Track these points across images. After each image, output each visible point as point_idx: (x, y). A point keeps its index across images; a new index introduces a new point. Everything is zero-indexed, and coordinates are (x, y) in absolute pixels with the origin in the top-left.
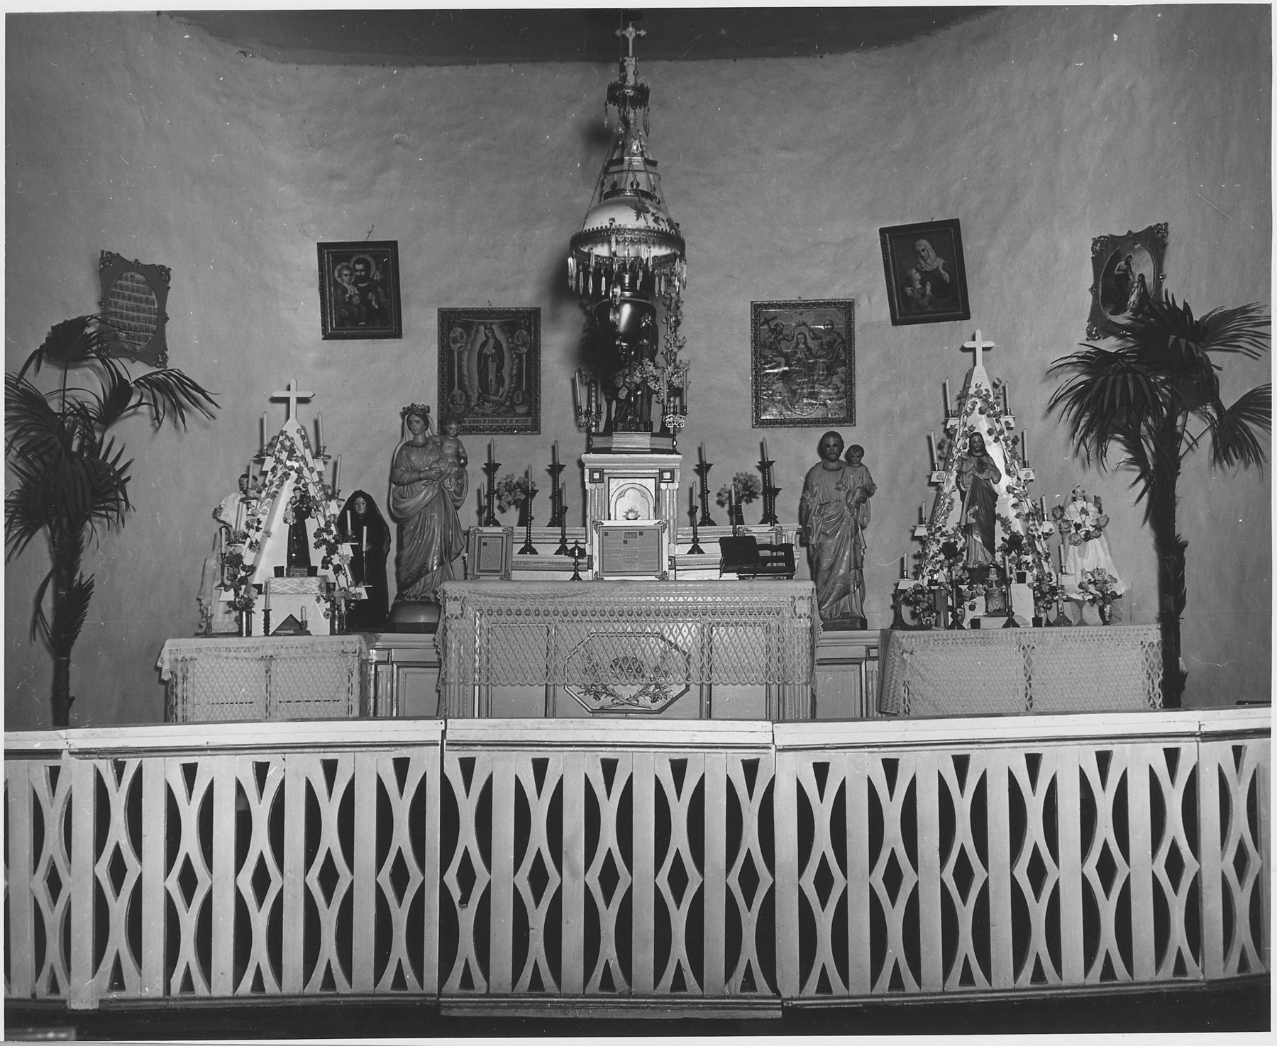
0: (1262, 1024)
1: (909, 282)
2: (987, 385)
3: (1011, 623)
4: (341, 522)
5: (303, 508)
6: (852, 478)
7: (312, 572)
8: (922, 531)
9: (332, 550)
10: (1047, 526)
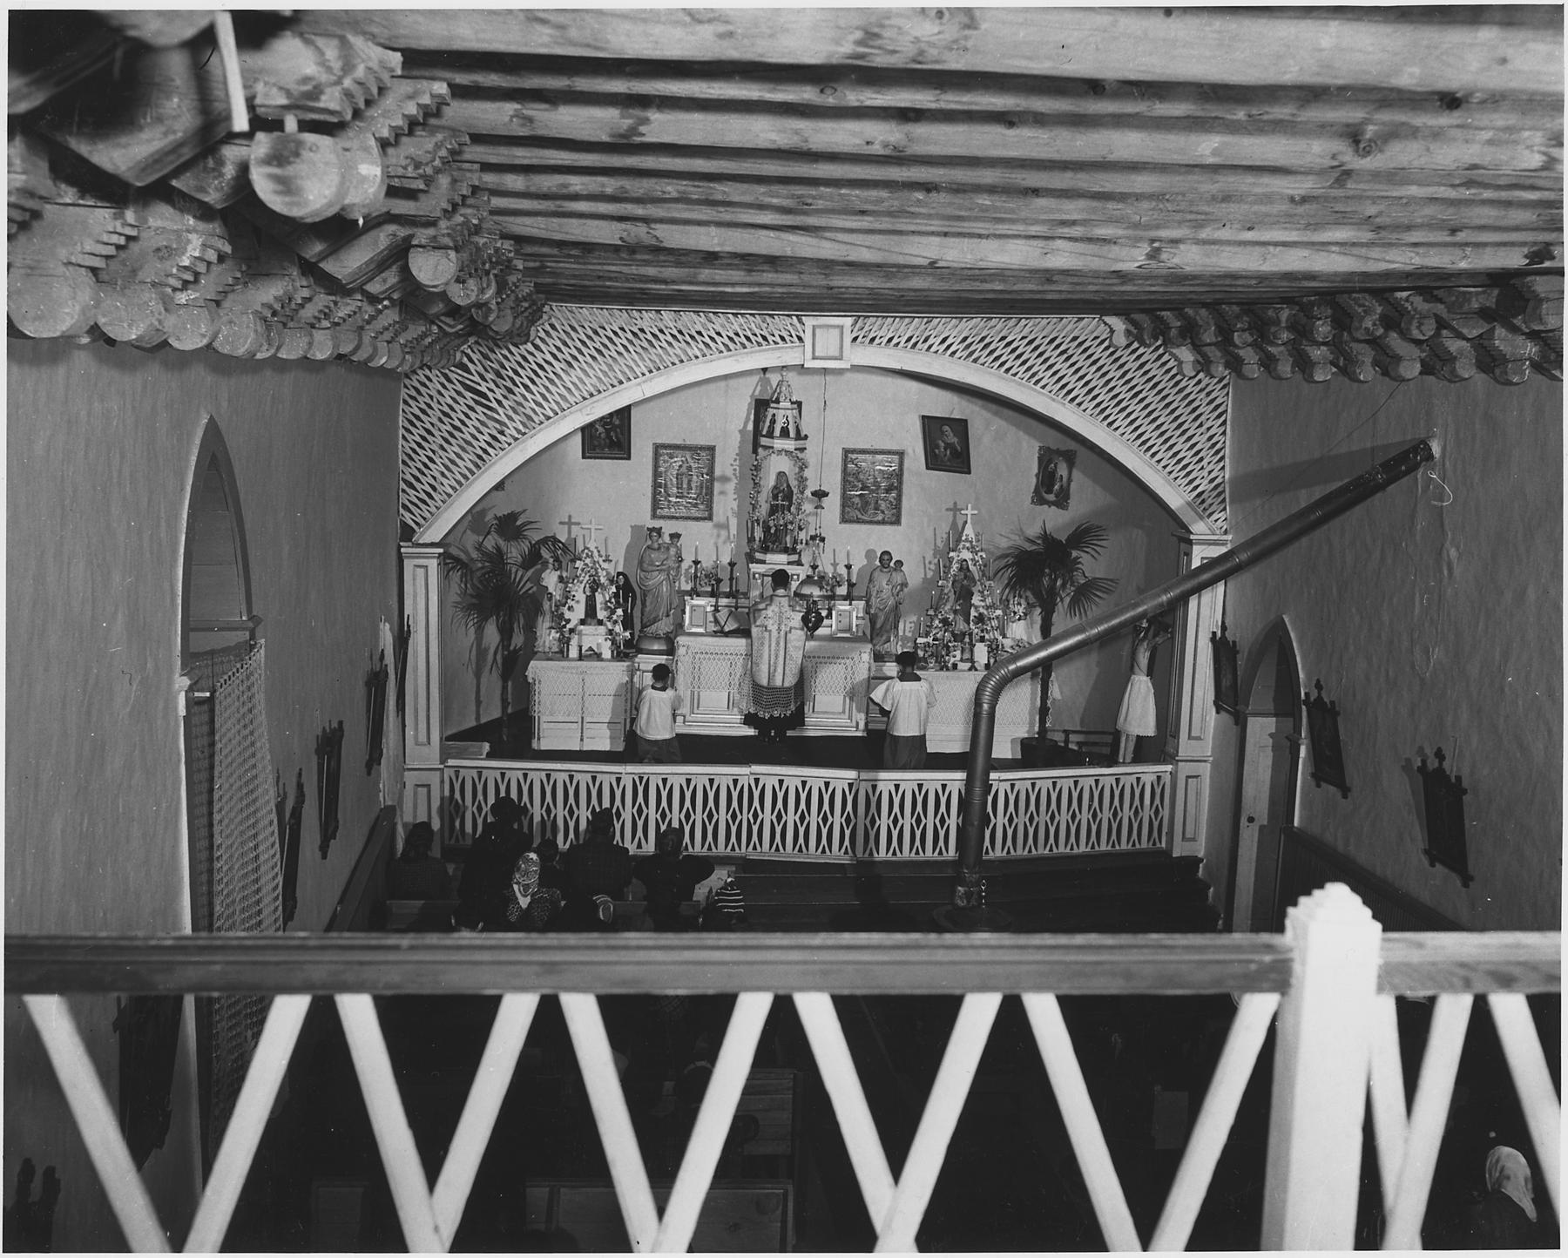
0: (18, 19)
1: (938, 447)
2: (972, 536)
3: (973, 668)
4: (616, 595)
5: (595, 586)
6: (897, 578)
7: (600, 623)
8: (931, 612)
9: (613, 612)
10: (999, 612)
